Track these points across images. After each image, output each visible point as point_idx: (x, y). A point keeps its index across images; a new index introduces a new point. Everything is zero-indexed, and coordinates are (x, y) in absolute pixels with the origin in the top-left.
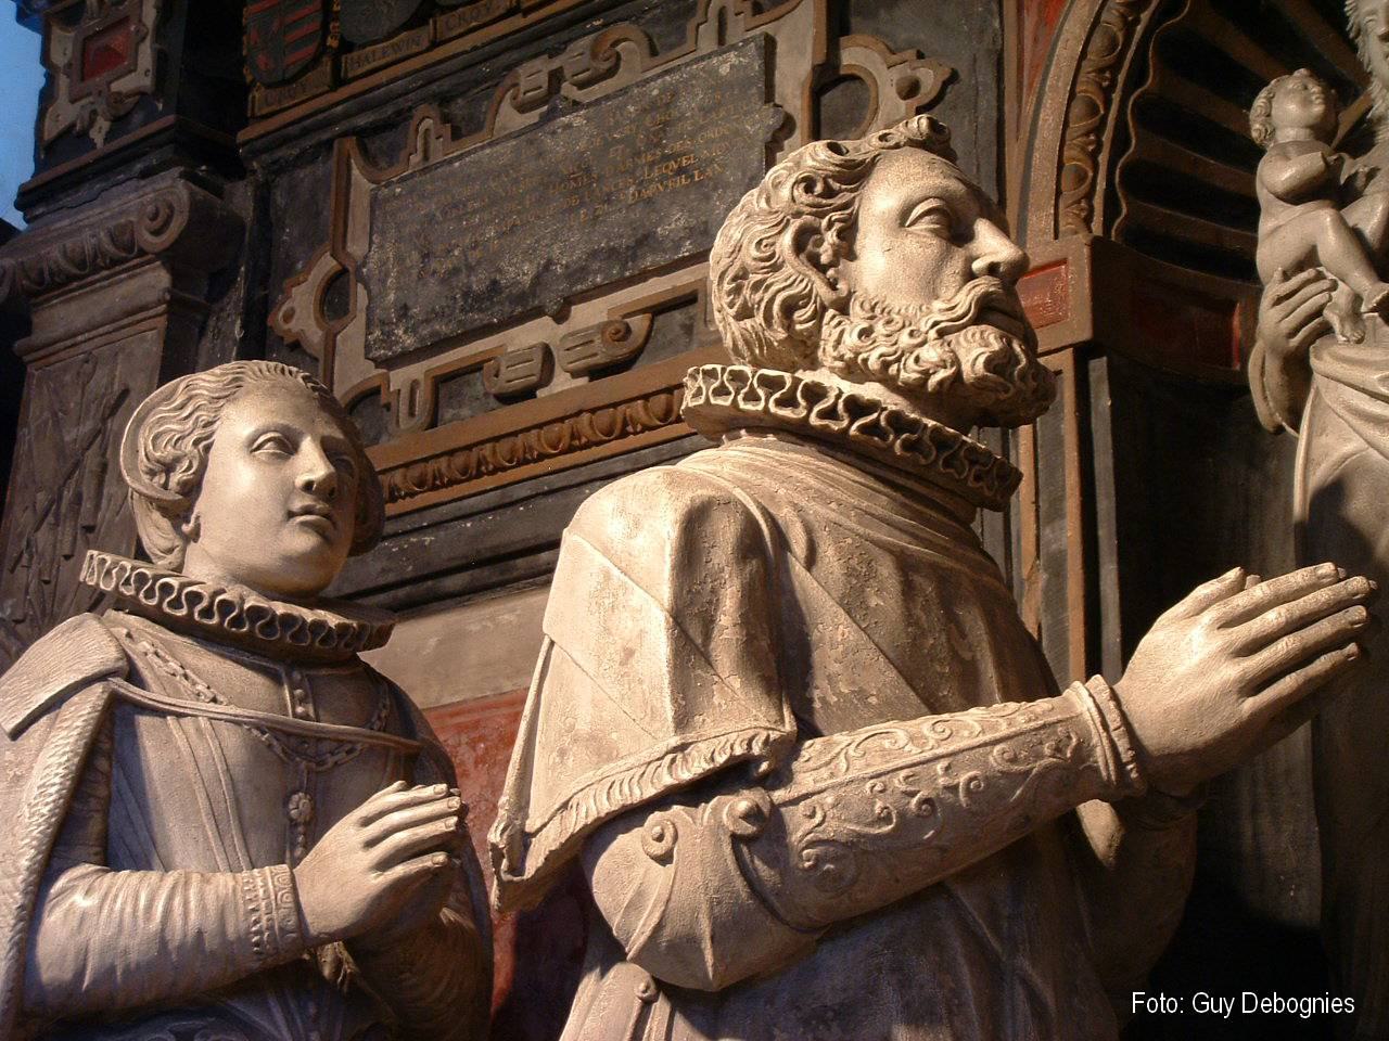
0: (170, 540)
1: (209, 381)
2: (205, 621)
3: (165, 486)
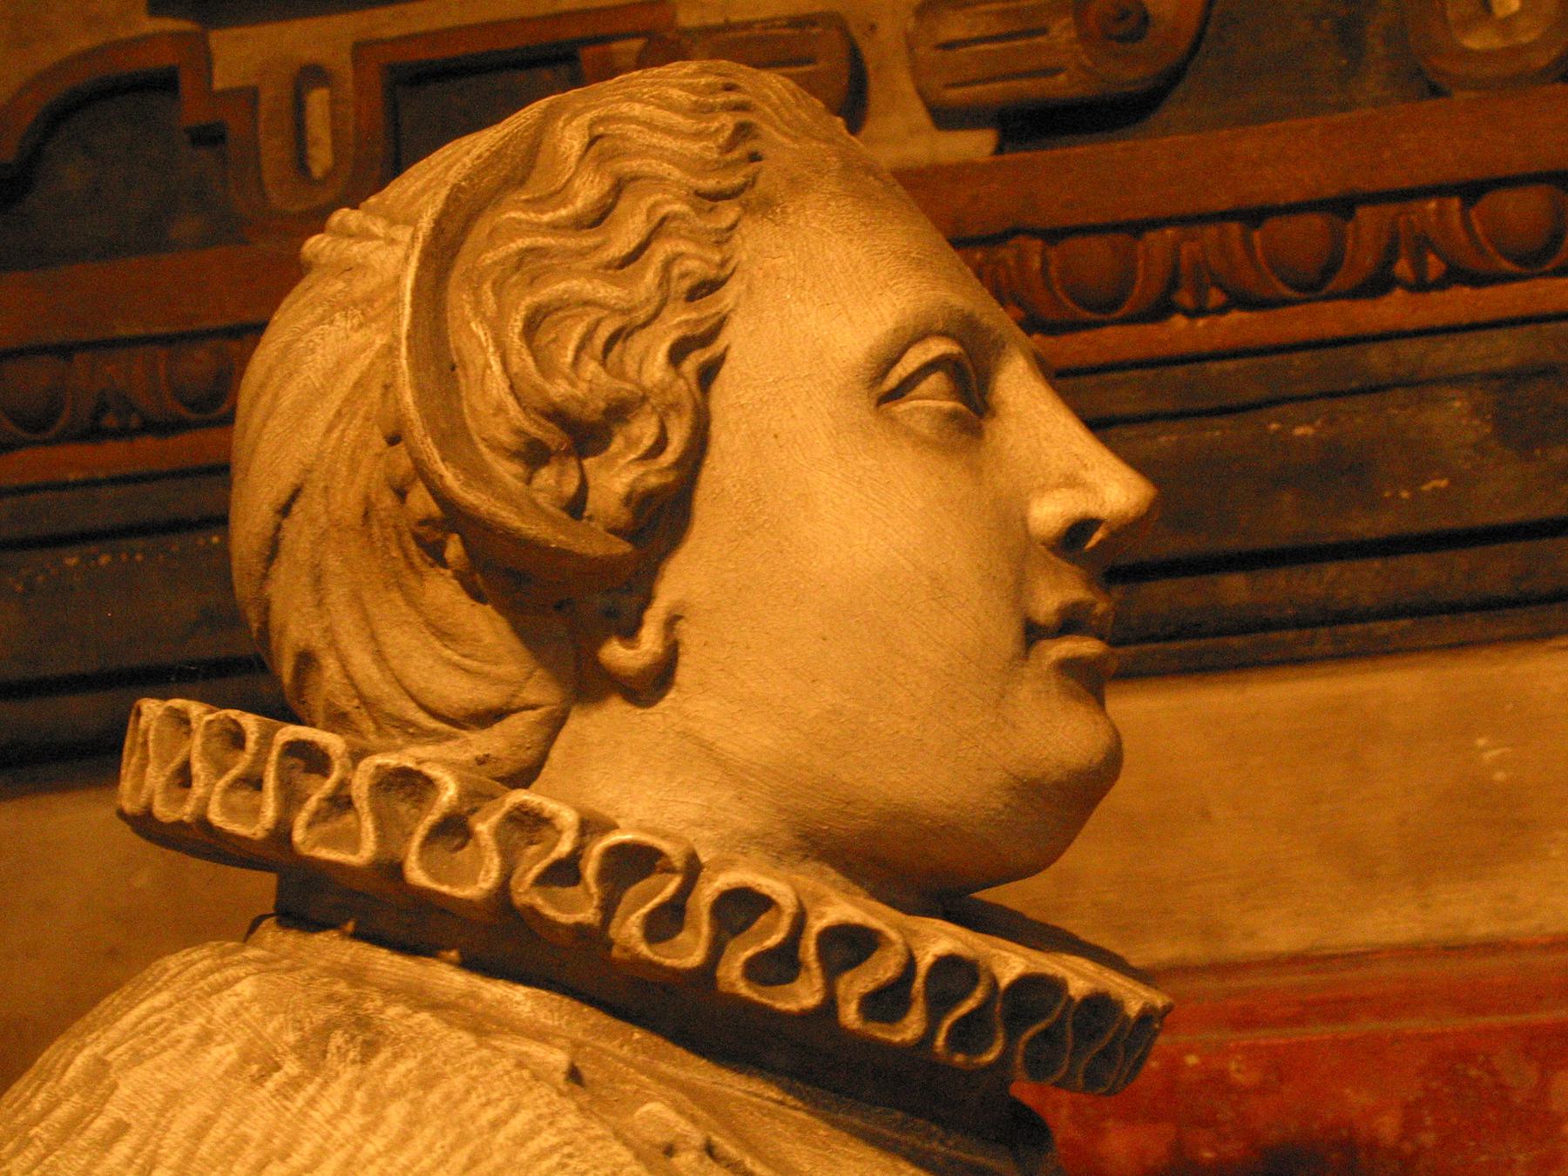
0: (498, 681)
1: (669, 131)
2: (880, 1032)
3: (576, 506)
